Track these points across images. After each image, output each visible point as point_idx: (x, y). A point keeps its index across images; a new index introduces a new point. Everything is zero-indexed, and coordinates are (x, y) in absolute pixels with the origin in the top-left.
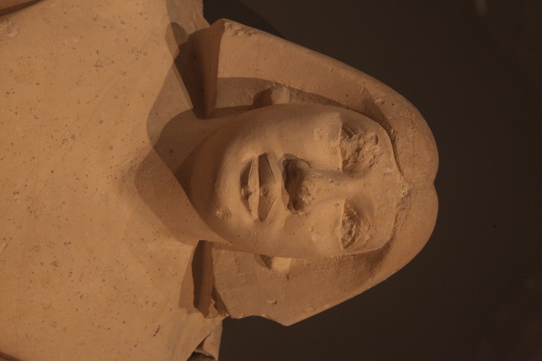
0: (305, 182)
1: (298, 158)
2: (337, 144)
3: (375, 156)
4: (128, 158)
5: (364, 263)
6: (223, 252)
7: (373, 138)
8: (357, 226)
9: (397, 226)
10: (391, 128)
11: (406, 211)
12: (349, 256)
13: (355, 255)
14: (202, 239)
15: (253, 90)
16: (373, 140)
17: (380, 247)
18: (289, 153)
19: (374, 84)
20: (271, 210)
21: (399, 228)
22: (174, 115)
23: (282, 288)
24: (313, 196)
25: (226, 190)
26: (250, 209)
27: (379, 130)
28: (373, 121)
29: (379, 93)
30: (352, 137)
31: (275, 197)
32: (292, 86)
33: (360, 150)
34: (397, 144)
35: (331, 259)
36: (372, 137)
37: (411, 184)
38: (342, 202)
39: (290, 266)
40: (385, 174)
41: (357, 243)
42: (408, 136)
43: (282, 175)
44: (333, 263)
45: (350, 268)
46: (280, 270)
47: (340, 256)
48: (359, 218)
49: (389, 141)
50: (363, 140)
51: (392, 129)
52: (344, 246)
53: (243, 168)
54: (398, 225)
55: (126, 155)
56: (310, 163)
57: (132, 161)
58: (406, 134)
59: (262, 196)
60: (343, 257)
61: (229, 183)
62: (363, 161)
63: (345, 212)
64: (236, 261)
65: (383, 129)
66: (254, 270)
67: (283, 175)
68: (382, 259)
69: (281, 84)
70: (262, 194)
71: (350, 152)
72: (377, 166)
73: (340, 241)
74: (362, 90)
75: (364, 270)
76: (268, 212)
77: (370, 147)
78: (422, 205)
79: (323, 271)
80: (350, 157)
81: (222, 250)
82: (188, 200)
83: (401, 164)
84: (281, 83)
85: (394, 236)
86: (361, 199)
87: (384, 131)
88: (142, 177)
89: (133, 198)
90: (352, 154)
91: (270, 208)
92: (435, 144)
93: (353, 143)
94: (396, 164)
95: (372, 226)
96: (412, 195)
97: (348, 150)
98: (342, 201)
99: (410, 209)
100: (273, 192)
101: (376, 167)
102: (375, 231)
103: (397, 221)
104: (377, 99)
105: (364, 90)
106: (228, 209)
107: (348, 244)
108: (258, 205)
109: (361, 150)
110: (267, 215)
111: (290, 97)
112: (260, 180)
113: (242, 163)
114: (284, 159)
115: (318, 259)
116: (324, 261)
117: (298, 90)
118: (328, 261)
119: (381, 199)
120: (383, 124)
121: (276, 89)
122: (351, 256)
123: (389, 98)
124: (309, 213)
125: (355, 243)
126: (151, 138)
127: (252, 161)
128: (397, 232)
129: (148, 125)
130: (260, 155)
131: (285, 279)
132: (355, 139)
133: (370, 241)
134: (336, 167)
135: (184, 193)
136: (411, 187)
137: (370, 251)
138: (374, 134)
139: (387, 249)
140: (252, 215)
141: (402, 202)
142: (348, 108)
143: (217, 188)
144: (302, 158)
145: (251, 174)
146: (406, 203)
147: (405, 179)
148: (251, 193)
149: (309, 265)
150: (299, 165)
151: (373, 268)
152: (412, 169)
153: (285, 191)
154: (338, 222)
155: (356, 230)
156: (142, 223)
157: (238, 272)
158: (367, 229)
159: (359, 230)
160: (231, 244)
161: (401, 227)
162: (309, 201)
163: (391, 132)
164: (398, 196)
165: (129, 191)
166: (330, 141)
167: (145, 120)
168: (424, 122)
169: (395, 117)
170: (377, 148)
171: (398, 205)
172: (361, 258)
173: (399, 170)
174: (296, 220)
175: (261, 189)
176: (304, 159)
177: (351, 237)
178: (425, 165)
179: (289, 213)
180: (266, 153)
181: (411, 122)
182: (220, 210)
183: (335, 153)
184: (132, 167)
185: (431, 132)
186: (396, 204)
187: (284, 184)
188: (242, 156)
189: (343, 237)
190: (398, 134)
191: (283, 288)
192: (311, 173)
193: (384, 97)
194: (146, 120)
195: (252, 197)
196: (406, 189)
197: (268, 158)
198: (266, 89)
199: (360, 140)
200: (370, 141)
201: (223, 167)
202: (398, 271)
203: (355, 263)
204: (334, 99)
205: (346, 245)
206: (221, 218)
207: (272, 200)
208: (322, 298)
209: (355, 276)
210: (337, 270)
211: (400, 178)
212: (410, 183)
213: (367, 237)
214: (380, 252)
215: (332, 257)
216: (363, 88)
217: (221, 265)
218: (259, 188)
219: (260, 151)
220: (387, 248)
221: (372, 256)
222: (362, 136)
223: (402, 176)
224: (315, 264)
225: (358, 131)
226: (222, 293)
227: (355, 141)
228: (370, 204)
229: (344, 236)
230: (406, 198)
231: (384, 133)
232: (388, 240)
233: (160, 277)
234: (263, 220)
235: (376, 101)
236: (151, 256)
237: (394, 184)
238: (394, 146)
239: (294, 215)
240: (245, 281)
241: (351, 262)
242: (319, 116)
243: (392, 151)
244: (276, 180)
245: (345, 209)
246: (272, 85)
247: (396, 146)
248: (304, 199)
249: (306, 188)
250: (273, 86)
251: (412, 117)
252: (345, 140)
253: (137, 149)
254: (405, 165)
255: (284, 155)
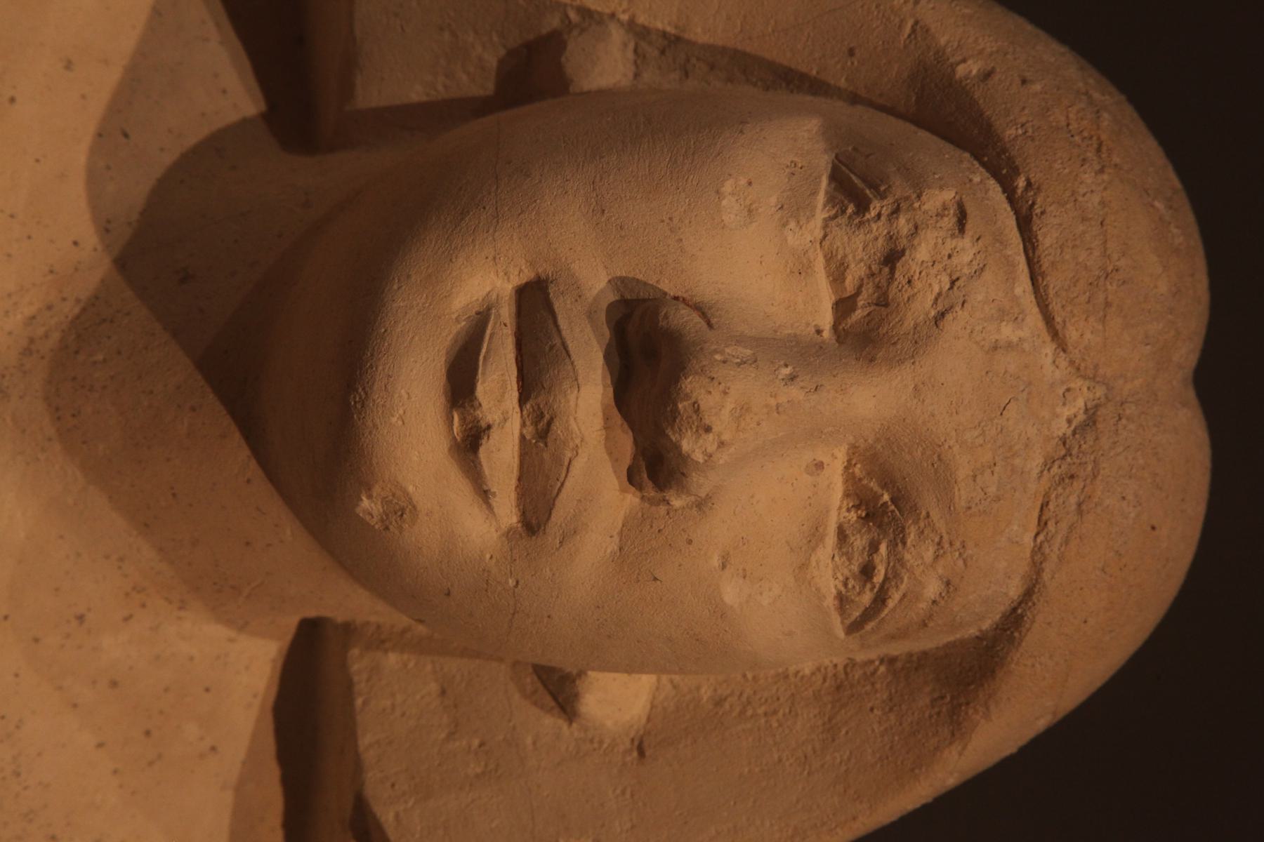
0: (689, 380)
1: (665, 294)
2: (809, 238)
3: (954, 277)
4: (15, 304)
5: (927, 689)
6: (392, 659)
7: (946, 212)
8: (893, 546)
9: (1046, 545)
10: (1016, 171)
11: (1078, 485)
12: (872, 662)
13: (892, 661)
14: (312, 613)
15: (495, 39)
16: (946, 219)
17: (986, 625)
18: (631, 275)
19: (953, 5)
20: (564, 491)
21: (1056, 549)
22: (192, 140)
23: (618, 791)
24: (719, 436)
25: (394, 420)
26: (485, 488)
27: (971, 180)
28: (948, 148)
29: (970, 40)
30: (867, 209)
31: (578, 441)
32: (642, 19)
33: (899, 258)
34: (1038, 232)
35: (803, 677)
36: (945, 208)
37: (1098, 382)
38: (834, 457)
39: (649, 707)
40: (995, 348)
41: (894, 610)
42: (1080, 199)
43: (604, 357)
44: (811, 693)
45: (875, 711)
46: (609, 723)
47: (836, 666)
48: (898, 514)
49: (1009, 222)
50: (908, 221)
51: (1019, 174)
52: (848, 622)
53: (458, 333)
54: (1048, 541)
55: (9, 295)
56: (710, 308)
57: (34, 317)
58: (1073, 193)
59: (528, 437)
60: (849, 670)
61: (403, 391)
62: (909, 299)
63: (847, 495)
64: (443, 692)
65: (987, 175)
66: (511, 724)
67: (607, 357)
68: (993, 672)
69: (599, 13)
70: (529, 431)
71: (862, 264)
72: (962, 315)
73: (830, 602)
74: (908, 30)
75: (927, 715)
76: (554, 500)
77: (936, 244)
78: (1141, 461)
79: (775, 725)
80: (861, 286)
81: (386, 651)
82: (253, 464)
83: (1055, 306)
84: (599, 9)
85: (1036, 580)
86: (905, 444)
87: (992, 183)
88: (74, 379)
89: (38, 460)
90: (868, 272)
91: (562, 484)
92: (1194, 229)
93: (870, 231)
94: (1036, 310)
95: (951, 544)
96: (1100, 426)
97: (854, 257)
98: (836, 452)
99: (1095, 477)
100: (572, 421)
101: (956, 324)
102: (960, 563)
103: (1046, 524)
104: (964, 61)
105: (913, 30)
106: (406, 493)
107: (861, 616)
108: (516, 473)
109: (903, 259)
110: (551, 510)
111: (635, 62)
112: (521, 377)
113: (454, 317)
114: (612, 297)
115: (754, 678)
116: (776, 683)
117: (664, 35)
118: (793, 686)
119: (980, 441)
120: (986, 159)
121: (583, 30)
122: (877, 663)
123: (1009, 56)
124: (708, 497)
125: (886, 611)
126: (105, 229)
127: (489, 309)
128: (1048, 567)
129: (93, 180)
130: (519, 283)
131: (628, 759)
132: (879, 216)
133: (943, 603)
134: (808, 324)
135: (237, 437)
136: (1098, 395)
137: (949, 643)
138: (953, 195)
139: (1012, 633)
140: (496, 510)
141: (1063, 452)
142: (854, 99)
143: (360, 414)
144: (679, 294)
145: (485, 357)
146: (1081, 455)
147: (1072, 363)
148: (489, 427)
149: (719, 702)
150: (666, 317)
151: (963, 708)
152: (1100, 327)
153: (617, 418)
154: (821, 530)
155: (889, 563)
156: (79, 555)
157: (450, 736)
158: (929, 555)
159: (901, 561)
160: (421, 629)
161: (1063, 549)
162: (705, 453)
163: (1017, 187)
164: (1049, 430)
165: (24, 431)
166: (785, 225)
167: (80, 156)
168: (1151, 146)
169: (1030, 130)
170: (963, 249)
171: (1048, 464)
172: (916, 669)
173: (1048, 332)
174: (662, 527)
175: (525, 412)
176: (685, 296)
177: (872, 589)
178: (1149, 311)
179: (637, 500)
180: (543, 276)
181: (1095, 146)
182: (375, 495)
183: (802, 270)
184: (32, 340)
185: (1177, 184)
186: (1042, 460)
187: (611, 390)
188: (452, 288)
189: (843, 589)
190: (1042, 194)
191: (623, 792)
192: (714, 347)
193: (991, 54)
194: (82, 159)
195: (491, 441)
196: (1080, 403)
197: (551, 295)
198: (544, 32)
199: (897, 218)
200: (937, 222)
201: (383, 330)
202: (1060, 715)
203: (893, 691)
204: (803, 68)
205: (853, 618)
206: (377, 527)
207: (569, 454)
208: (772, 825)
209: (896, 738)
210: (826, 719)
211: (1054, 362)
212: (1094, 378)
213: (932, 589)
214: (985, 643)
215: (807, 671)
216: (910, 23)
217: (384, 710)
218: (518, 409)
219: (521, 271)
220: (1012, 629)
221: (958, 661)
222: (904, 205)
223: (1062, 354)
224: (744, 699)
225: (890, 187)
226: (391, 816)
227: (880, 223)
228: (940, 459)
229: (845, 585)
230: (1077, 436)
231: (991, 193)
232: (1016, 598)
233: (151, 764)
234: (539, 527)
235: (961, 70)
236: (114, 684)
237: (1030, 383)
238: (1030, 240)
239: (654, 508)
240: (479, 770)
241: (878, 686)
242: (741, 132)
243: (1021, 260)
244: (580, 378)
245: (846, 482)
246: (567, 17)
247: (1037, 241)
248: (686, 445)
249: (695, 403)
250: (570, 22)
251: (1098, 128)
252: (842, 220)
253: (51, 272)
254: (1072, 312)
255: (609, 281)
